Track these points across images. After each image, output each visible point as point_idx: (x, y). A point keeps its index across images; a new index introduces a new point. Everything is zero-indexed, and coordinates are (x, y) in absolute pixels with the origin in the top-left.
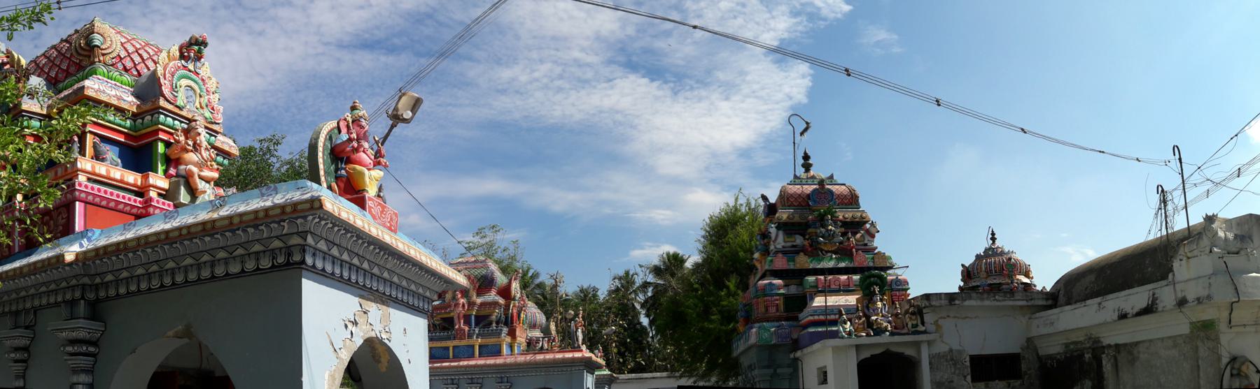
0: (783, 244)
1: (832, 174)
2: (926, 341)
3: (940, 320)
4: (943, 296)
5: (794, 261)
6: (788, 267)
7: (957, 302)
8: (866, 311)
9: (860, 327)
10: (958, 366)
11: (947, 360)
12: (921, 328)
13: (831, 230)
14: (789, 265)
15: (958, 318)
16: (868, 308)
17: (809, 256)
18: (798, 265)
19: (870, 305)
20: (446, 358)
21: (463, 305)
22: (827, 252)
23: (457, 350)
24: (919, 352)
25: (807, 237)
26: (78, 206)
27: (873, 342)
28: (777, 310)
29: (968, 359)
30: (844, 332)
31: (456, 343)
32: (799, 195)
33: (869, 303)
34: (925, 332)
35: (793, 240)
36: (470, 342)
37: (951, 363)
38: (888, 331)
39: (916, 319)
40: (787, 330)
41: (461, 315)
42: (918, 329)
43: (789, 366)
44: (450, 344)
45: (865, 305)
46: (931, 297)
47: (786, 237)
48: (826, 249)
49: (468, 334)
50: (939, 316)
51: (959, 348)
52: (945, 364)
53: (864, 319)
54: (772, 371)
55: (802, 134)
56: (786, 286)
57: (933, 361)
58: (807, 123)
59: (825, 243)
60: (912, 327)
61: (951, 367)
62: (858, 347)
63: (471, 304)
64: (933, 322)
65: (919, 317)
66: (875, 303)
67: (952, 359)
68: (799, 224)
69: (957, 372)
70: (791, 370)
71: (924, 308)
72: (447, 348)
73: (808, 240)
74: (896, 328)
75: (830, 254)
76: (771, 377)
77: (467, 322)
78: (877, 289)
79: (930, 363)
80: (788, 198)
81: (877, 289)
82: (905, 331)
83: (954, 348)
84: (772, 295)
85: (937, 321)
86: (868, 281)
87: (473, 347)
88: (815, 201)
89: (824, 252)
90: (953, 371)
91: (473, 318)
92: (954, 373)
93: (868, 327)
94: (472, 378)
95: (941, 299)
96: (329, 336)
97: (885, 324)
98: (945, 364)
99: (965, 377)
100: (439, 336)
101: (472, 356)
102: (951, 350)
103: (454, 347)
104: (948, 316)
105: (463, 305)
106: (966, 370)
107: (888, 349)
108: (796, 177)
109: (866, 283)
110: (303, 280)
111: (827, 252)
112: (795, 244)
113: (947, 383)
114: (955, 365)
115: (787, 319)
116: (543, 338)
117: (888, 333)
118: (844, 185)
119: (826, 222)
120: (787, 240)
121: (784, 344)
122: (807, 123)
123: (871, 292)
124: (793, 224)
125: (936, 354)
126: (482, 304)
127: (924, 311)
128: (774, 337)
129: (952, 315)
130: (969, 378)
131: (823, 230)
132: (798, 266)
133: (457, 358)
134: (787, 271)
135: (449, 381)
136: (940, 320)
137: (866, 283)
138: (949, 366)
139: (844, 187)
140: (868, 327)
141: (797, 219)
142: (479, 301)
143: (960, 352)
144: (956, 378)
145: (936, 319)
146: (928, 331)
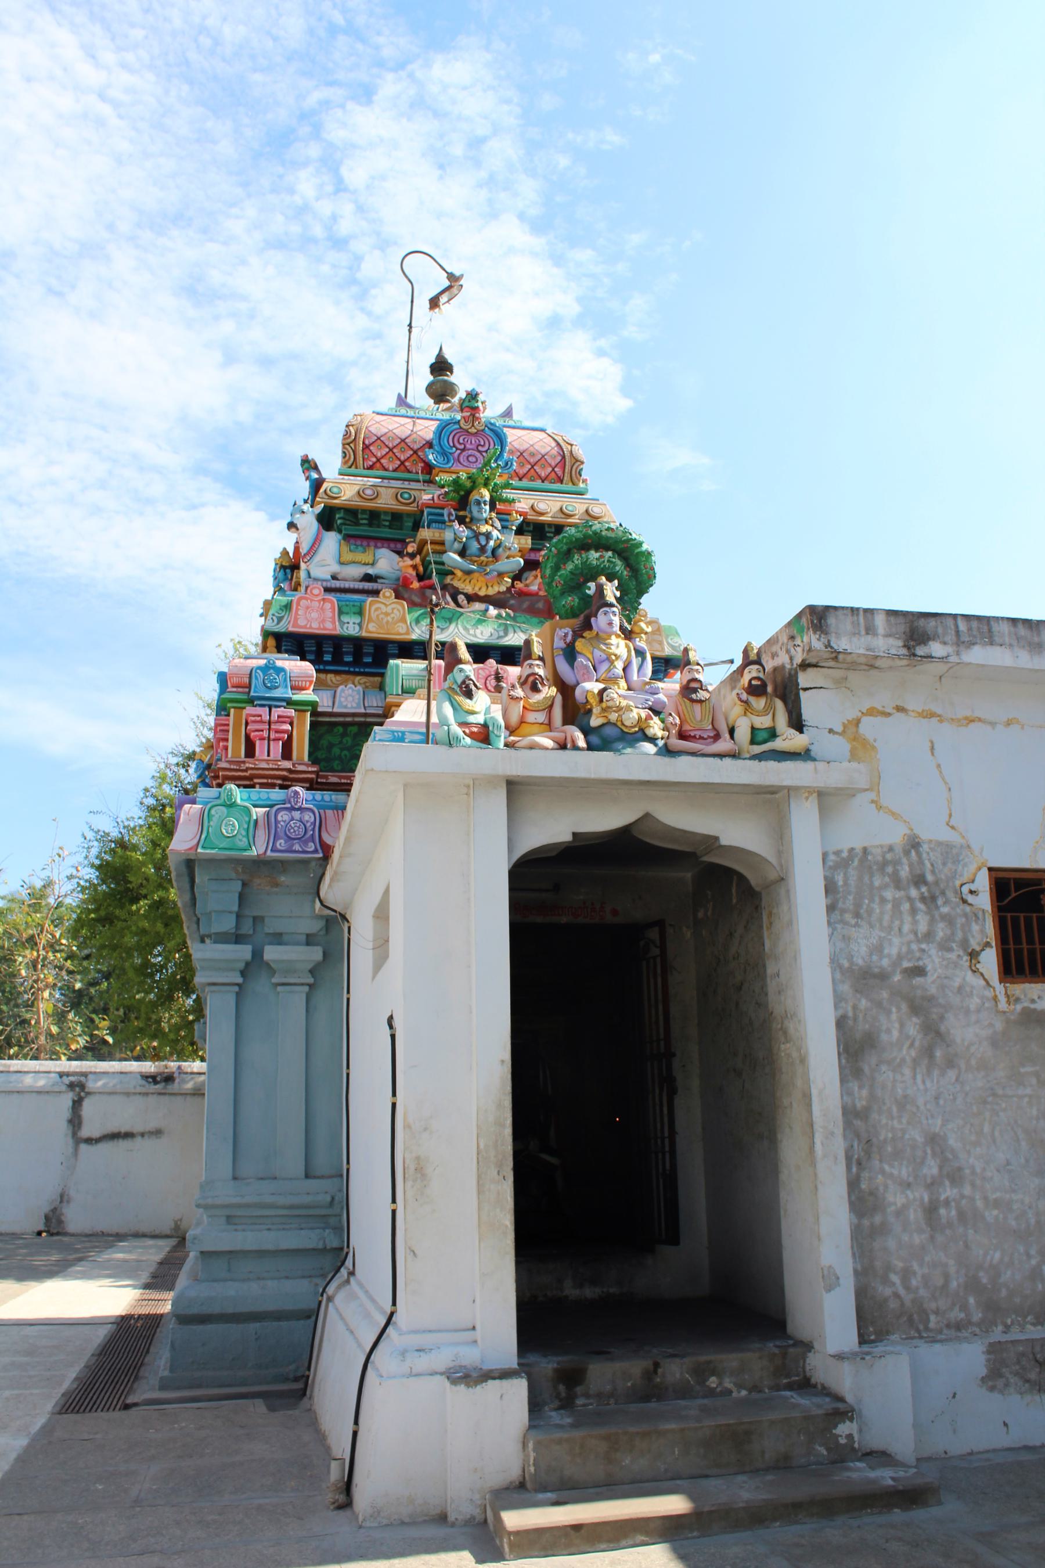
0: (335, 568)
1: (511, 405)
2: (810, 791)
3: (865, 720)
4: (880, 621)
5: (360, 613)
6: (339, 631)
7: (936, 648)
8: (563, 666)
9: (531, 717)
10: (945, 910)
11: (897, 883)
12: (789, 740)
13: (488, 536)
14: (342, 623)
15: (941, 718)
16: (571, 654)
17: (412, 604)
18: (372, 627)
19: (579, 645)
22: (471, 598)
24: (781, 832)
25: (411, 548)
27: (581, 774)
28: (287, 754)
29: (983, 883)
30: (463, 724)
32: (403, 441)
33: (578, 634)
34: (804, 755)
35: (367, 557)
37: (914, 893)
38: (652, 740)
39: (769, 709)
40: (308, 817)
42: (778, 744)
43: (310, 940)
45: (559, 644)
46: (831, 620)
47: (345, 548)
48: (469, 589)
50: (865, 706)
51: (945, 835)
52: (889, 894)
53: (549, 691)
54: (244, 952)
55: (434, 303)
56: (319, 686)
57: (840, 879)
58: (451, 277)
59: (468, 573)
60: (753, 742)
61: (914, 911)
62: (514, 788)
64: (839, 728)
65: (779, 704)
66: (600, 638)
67: (919, 880)
68: (396, 517)
69: (941, 931)
70: (316, 954)
71: (805, 666)
73: (412, 556)
74: (682, 736)
75: (478, 606)
76: (243, 973)
78: (611, 592)
79: (830, 888)
80: (366, 447)
81: (611, 592)
82: (724, 745)
83: (924, 835)
84: (271, 703)
85: (857, 722)
86: (577, 559)
88: (444, 454)
89: (461, 598)
90: (923, 927)
92: (929, 936)
93: (568, 720)
95: (870, 630)
97: (637, 713)
98: (889, 894)
99: (974, 955)
102: (914, 844)
104: (900, 709)
106: (975, 927)
107: (647, 816)
108: (402, 401)
109: (570, 566)
111: (471, 598)
112: (371, 571)
113: (897, 978)
114: (930, 900)
115: (312, 786)
117: (649, 748)
118: (543, 430)
119: (475, 509)
120: (348, 556)
121: (283, 862)
122: (451, 277)
123: (586, 600)
124: (374, 516)
125: (851, 850)
127: (804, 679)
128: (261, 835)
129: (914, 704)
130: (990, 961)
131: (463, 532)
132: (372, 630)
134: (337, 642)
136: (865, 720)
137: (570, 566)
138: (906, 906)
139: (542, 435)
140: (568, 720)
141: (386, 501)
143: (951, 853)
144: (934, 960)
145: (852, 714)
146: (815, 751)
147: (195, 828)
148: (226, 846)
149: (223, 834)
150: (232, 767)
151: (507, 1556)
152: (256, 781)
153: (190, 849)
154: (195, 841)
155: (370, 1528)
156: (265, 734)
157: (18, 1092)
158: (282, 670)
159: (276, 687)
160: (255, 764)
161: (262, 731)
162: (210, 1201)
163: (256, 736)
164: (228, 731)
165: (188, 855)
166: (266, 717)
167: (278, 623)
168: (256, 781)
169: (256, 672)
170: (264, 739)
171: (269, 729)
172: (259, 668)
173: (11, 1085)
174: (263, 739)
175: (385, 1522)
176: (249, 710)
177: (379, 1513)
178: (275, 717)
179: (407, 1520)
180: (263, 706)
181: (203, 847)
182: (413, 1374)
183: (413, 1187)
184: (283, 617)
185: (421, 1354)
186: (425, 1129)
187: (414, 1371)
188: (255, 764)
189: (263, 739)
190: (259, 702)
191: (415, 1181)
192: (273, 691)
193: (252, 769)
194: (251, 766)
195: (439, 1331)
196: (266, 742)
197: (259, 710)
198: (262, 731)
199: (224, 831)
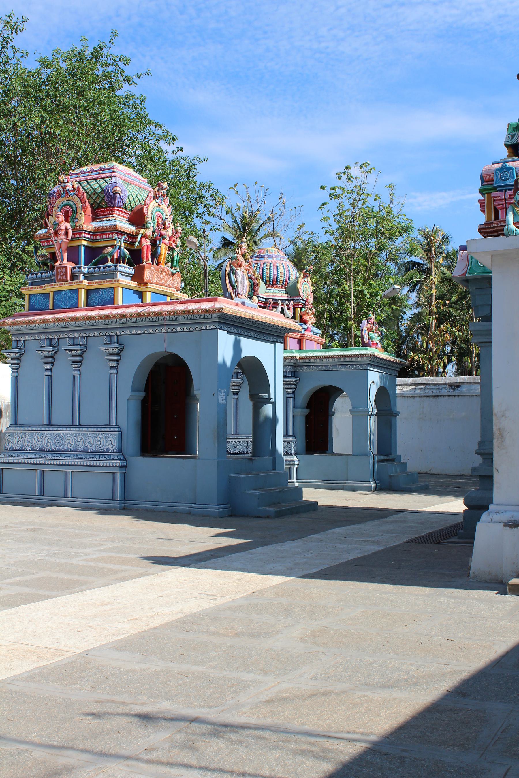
20: (44, 309)
21: (67, 233)
23: (74, 301)
26: (120, 290)
31: (57, 287)
36: (74, 286)
41: (64, 247)
44: (49, 289)
49: (72, 274)
63: (77, 231)
72: (47, 295)
77: (74, 258)
87: (76, 291)
91: (127, 259)
94: (74, 338)
96: (92, 714)
100: (41, 278)
101: (75, 307)
103: (55, 293)
105: (67, 233)
110: (467, 508)
116: (289, 301)
126: (97, 232)
133: (57, 309)
135: (47, 342)
142: (90, 226)
147: (465, 263)
148: (481, 272)
149: (479, 265)
150: (486, 227)
151: (508, 594)
152: (500, 233)
153: (462, 275)
154: (465, 270)
155: (473, 582)
156: (504, 206)
157: (476, 395)
158: (510, 168)
159: (508, 179)
160: (498, 224)
161: (502, 204)
162: (482, 451)
163: (499, 208)
164: (484, 206)
165: (462, 278)
166: (502, 197)
167: (512, 139)
168: (500, 233)
169: (496, 172)
170: (503, 209)
171: (506, 203)
172: (498, 170)
173: (472, 391)
174: (502, 209)
175: (479, 580)
176: (494, 194)
177: (476, 576)
178: (507, 196)
179: (488, 581)
180: (501, 190)
181: (469, 273)
182: (492, 522)
183: (497, 441)
184: (515, 134)
185: (497, 514)
186: (503, 416)
187: (493, 520)
188: (498, 224)
189: (502, 209)
190: (499, 189)
191: (498, 439)
192: (506, 182)
193: (496, 227)
194: (495, 225)
195: (509, 505)
196: (505, 210)
197: (499, 194)
198: (502, 204)
199: (479, 263)
